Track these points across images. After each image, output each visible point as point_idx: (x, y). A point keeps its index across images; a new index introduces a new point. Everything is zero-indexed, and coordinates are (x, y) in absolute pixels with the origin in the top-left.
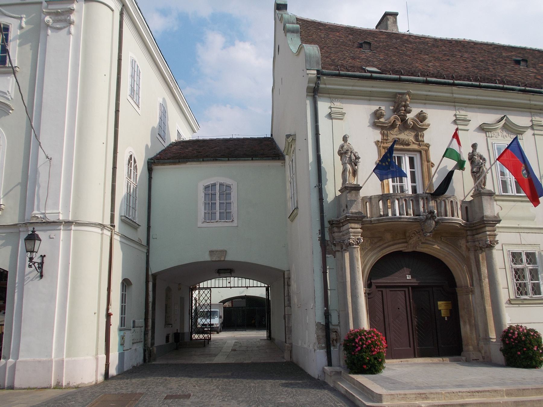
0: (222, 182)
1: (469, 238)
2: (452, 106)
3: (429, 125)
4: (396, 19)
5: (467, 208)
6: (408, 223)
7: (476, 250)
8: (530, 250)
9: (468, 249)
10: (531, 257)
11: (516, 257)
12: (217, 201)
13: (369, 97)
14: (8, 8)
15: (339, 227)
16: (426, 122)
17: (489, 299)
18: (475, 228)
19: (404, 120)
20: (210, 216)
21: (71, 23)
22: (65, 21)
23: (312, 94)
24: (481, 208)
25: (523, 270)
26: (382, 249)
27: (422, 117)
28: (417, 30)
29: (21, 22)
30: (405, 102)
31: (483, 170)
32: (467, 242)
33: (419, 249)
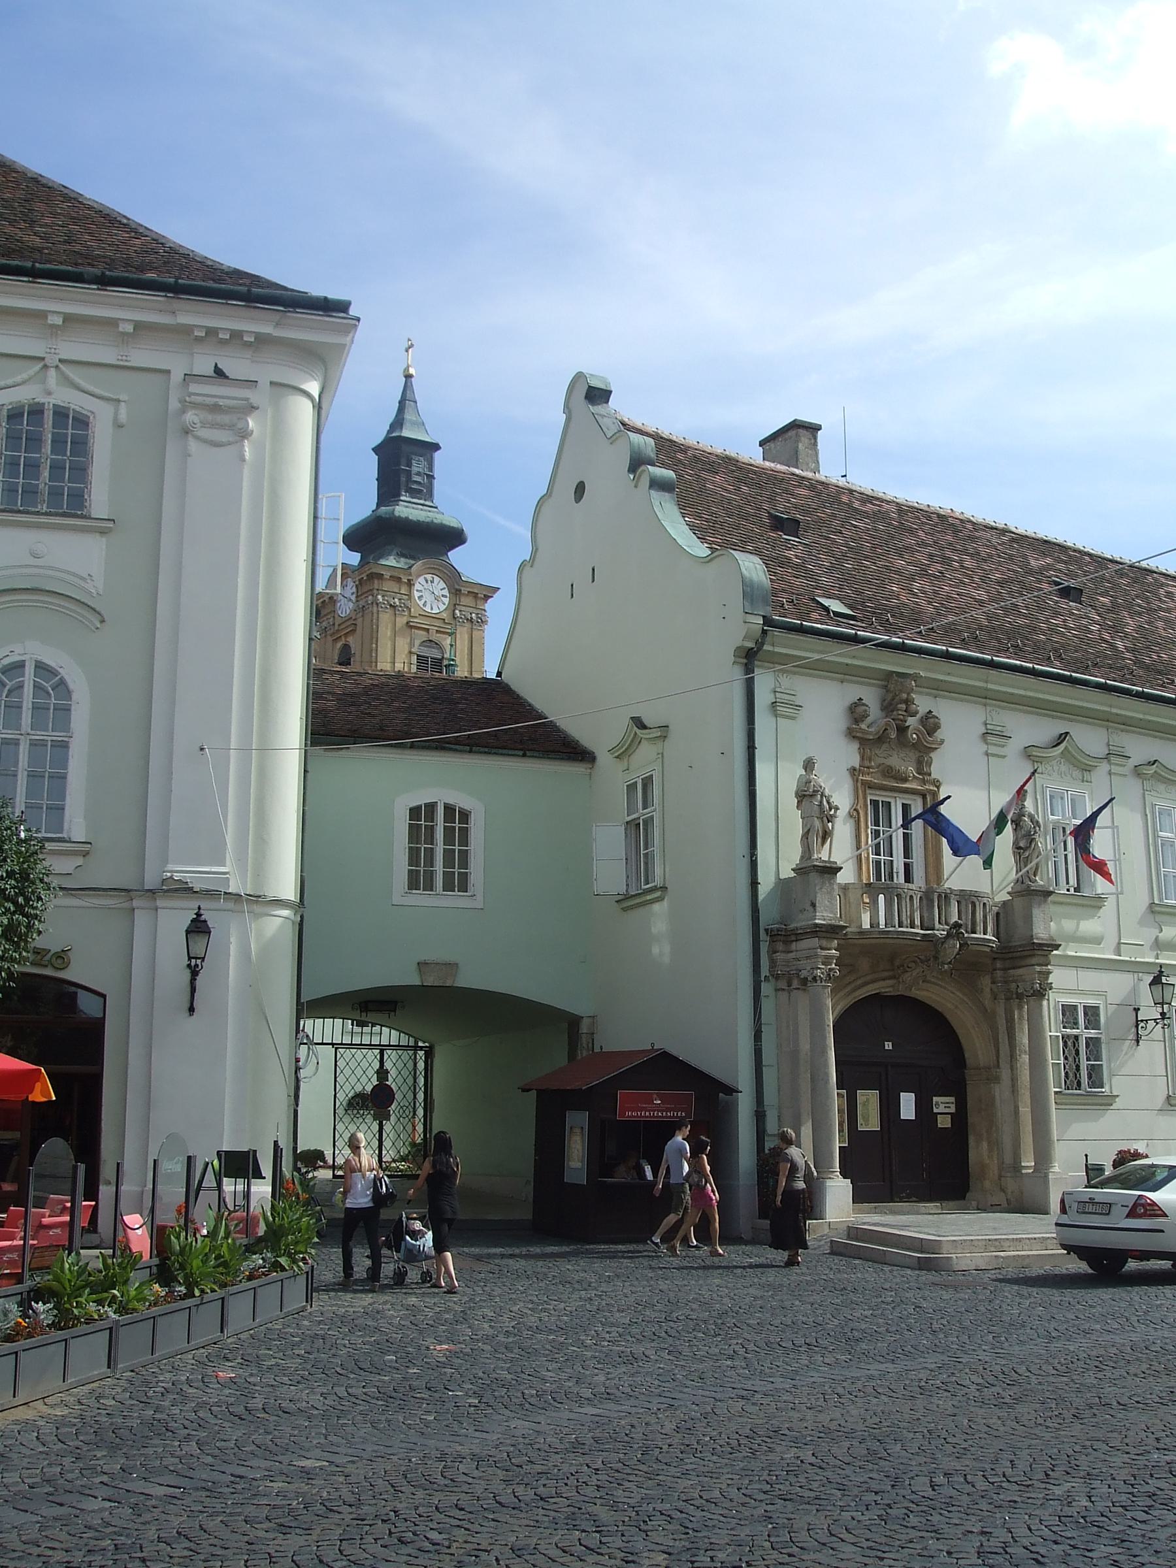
0: (451, 801)
1: (999, 973)
2: (980, 703)
3: (942, 742)
4: (815, 438)
5: (1003, 916)
6: (909, 942)
7: (1007, 999)
8: (1091, 1001)
9: (995, 997)
10: (1092, 1013)
11: (1069, 1012)
12: (438, 845)
13: (845, 673)
14: (93, 371)
15: (787, 942)
16: (939, 735)
17: (1028, 1093)
18: (1010, 955)
19: (902, 730)
20: (418, 880)
21: (244, 434)
22: (231, 427)
23: (745, 661)
24: (1028, 919)
25: (1076, 1037)
26: (854, 990)
27: (930, 724)
28: (863, 480)
29: (116, 414)
30: (908, 694)
31: (1036, 844)
32: (993, 983)
33: (916, 993)
